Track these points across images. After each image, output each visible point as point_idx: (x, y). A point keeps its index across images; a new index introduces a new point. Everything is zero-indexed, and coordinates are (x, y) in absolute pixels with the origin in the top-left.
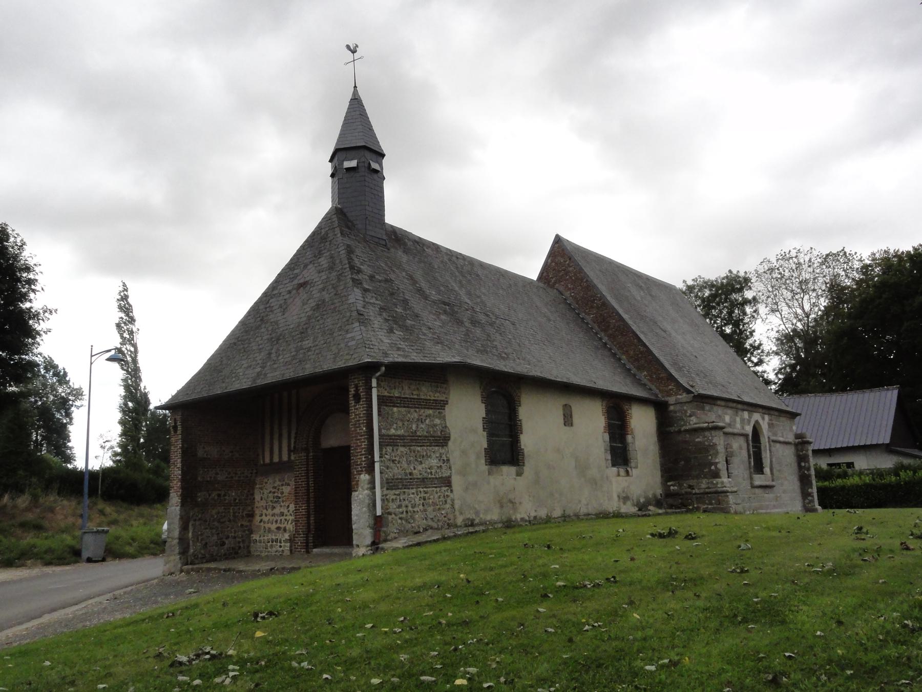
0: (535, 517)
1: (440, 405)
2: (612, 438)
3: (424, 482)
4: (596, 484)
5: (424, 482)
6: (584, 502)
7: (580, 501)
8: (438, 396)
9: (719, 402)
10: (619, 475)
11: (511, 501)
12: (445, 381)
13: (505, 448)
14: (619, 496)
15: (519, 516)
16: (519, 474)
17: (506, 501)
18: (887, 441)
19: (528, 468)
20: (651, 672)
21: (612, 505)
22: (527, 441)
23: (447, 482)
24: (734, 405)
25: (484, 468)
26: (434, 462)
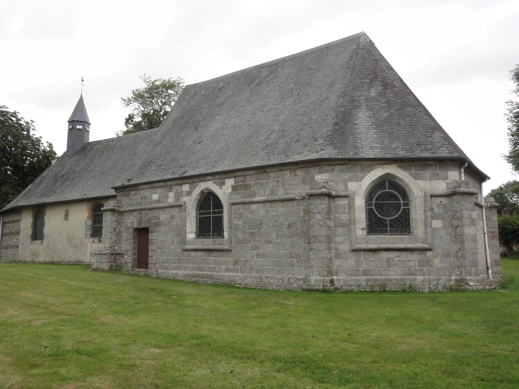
0: (44, 261)
1: (19, 221)
2: (34, 228)
3: (12, 247)
4: (77, 247)
5: (12, 247)
6: (69, 255)
7: (66, 255)
8: (19, 218)
9: (142, 187)
10: (94, 242)
11: (36, 254)
12: (21, 213)
13: (37, 234)
14: (91, 254)
15: (38, 260)
16: (42, 244)
17: (35, 254)
18: (433, 226)
19: (45, 241)
20: (513, 250)
21: (87, 259)
22: (46, 230)
23: (18, 247)
24: (162, 184)
25: (29, 241)
26: (15, 240)
